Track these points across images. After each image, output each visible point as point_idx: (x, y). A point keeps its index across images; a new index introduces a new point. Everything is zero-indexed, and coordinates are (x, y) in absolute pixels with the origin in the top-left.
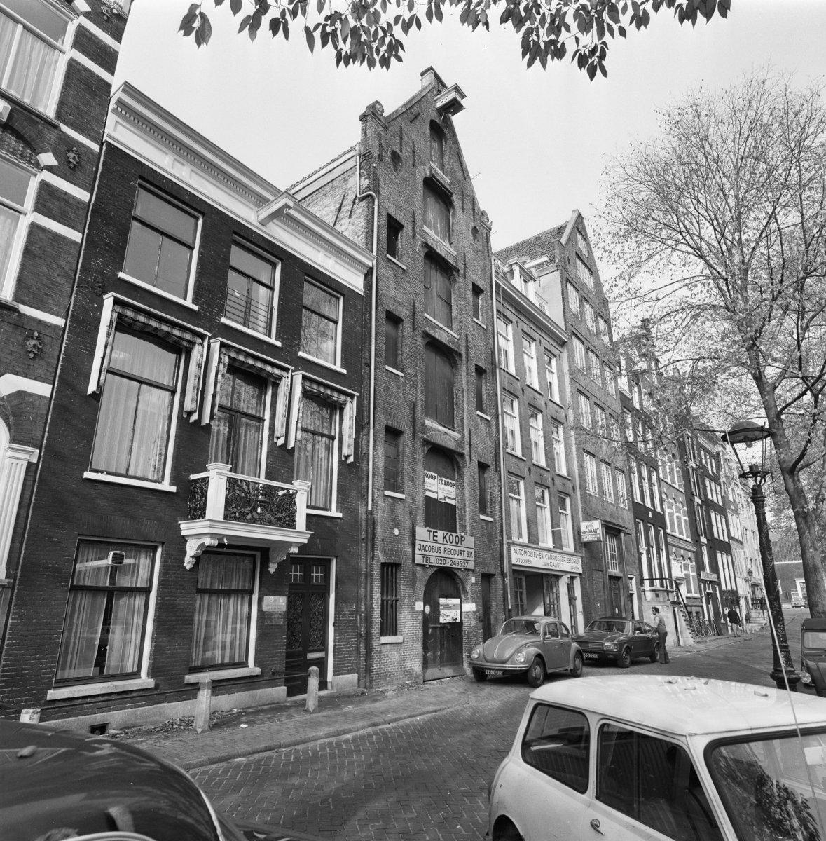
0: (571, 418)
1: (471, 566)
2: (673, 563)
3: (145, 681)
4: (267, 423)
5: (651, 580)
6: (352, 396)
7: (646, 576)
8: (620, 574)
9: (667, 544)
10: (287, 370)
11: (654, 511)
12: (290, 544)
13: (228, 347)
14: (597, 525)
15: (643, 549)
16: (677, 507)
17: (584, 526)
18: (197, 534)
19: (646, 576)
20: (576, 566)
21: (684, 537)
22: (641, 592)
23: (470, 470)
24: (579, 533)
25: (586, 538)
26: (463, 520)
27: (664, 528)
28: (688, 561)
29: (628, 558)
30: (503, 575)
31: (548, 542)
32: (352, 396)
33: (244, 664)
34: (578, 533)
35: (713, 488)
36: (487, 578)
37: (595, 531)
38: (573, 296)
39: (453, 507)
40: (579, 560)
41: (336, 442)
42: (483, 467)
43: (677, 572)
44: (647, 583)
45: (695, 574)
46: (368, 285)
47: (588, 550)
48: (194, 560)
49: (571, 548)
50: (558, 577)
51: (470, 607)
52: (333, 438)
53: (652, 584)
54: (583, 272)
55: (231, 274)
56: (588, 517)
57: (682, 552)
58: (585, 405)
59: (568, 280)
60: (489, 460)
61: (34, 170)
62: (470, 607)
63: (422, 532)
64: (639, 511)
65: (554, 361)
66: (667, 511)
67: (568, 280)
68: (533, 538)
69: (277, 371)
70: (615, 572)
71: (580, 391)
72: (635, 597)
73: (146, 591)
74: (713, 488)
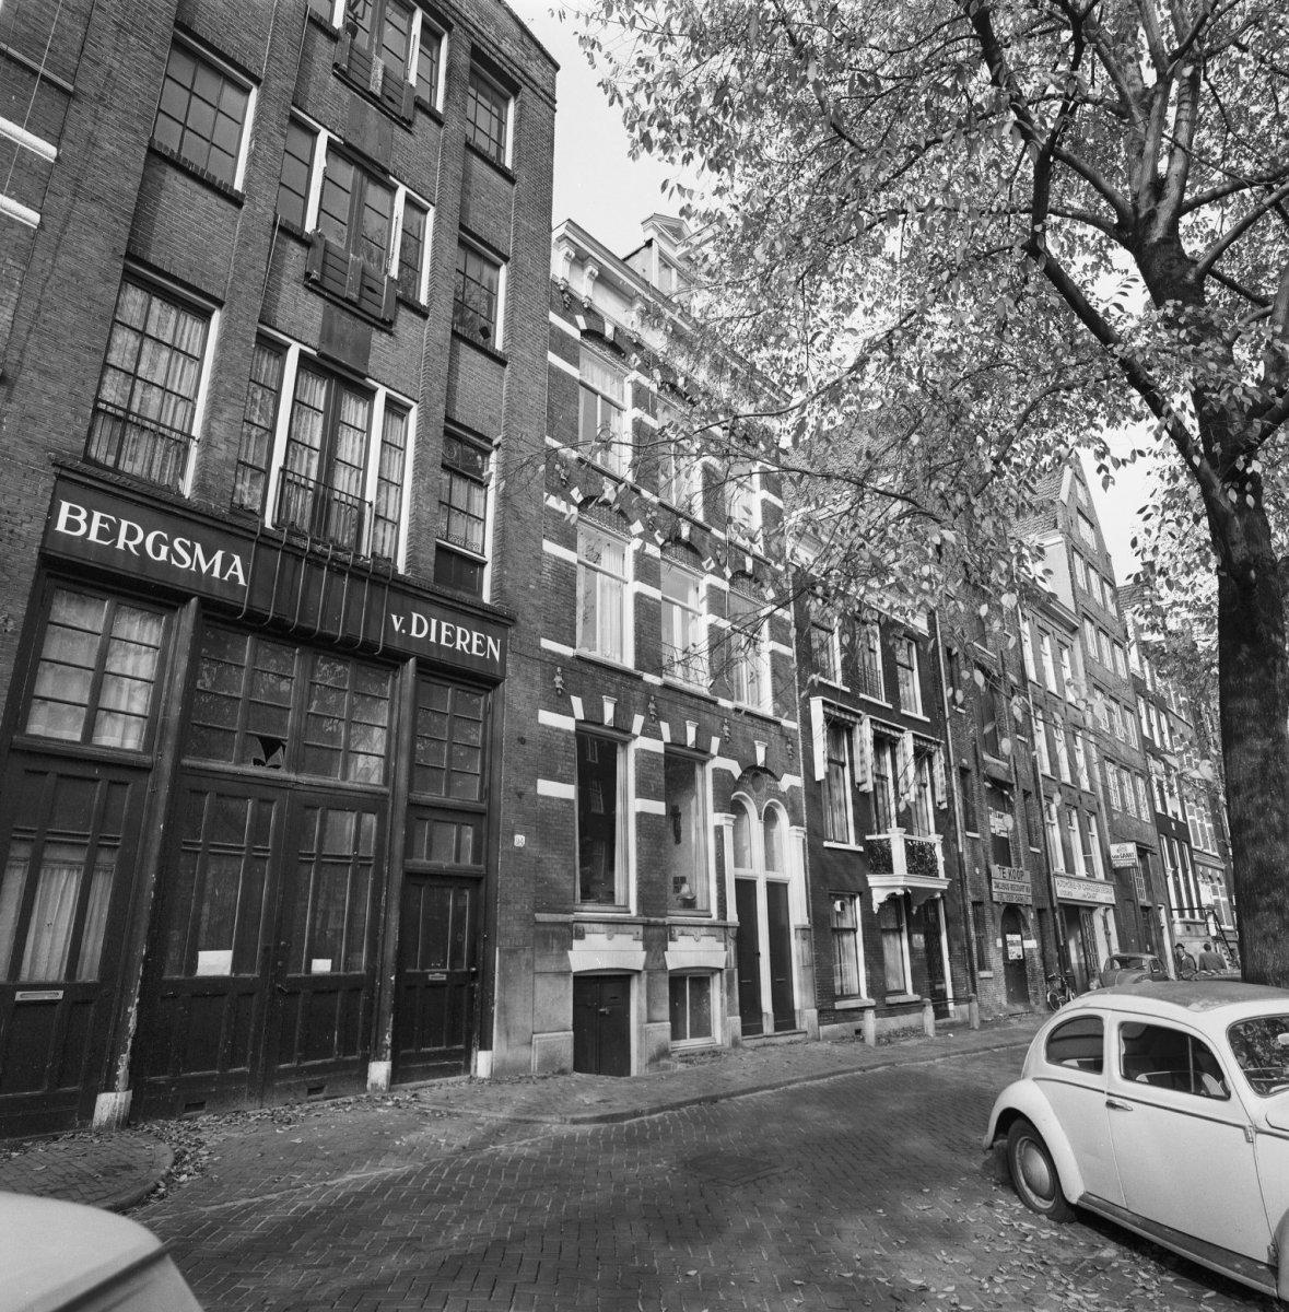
0: (1089, 722)
1: (1030, 901)
2: (1201, 886)
3: (911, 996)
4: (891, 781)
5: (1181, 910)
6: (938, 744)
7: (1174, 905)
8: (1149, 904)
9: (1193, 863)
10: (902, 731)
11: (1177, 822)
12: (936, 890)
13: (877, 723)
14: (1131, 848)
15: (1169, 868)
16: (1200, 813)
17: (1114, 849)
18: (880, 887)
19: (1174, 905)
20: (1106, 895)
21: (1210, 851)
22: (1171, 924)
23: (1016, 798)
24: (1109, 857)
25: (1118, 864)
26: (1017, 853)
27: (1189, 843)
28: (1216, 883)
29: (1154, 883)
30: (1053, 909)
31: (1081, 870)
32: (938, 744)
33: (903, 992)
34: (1107, 858)
35: (1154, 721)
36: (1040, 912)
37: (1129, 855)
38: (1079, 563)
39: (1006, 840)
40: (1111, 889)
41: (847, 769)
42: (1026, 794)
43: (1207, 898)
44: (1175, 913)
45: (1225, 899)
46: (932, 625)
47: (1117, 875)
48: (592, 890)
49: (1100, 875)
50: (1091, 909)
51: (1032, 944)
52: (843, 765)
53: (1182, 915)
54: (1084, 529)
55: (900, 669)
56: (1119, 837)
57: (1210, 871)
58: (1099, 701)
59: (1074, 549)
60: (1031, 788)
61: (699, 573)
62: (1032, 944)
63: (995, 868)
64: (1162, 822)
65: (1065, 653)
66: (1189, 818)
67: (1074, 549)
68: (1070, 867)
69: (893, 733)
70: (1144, 900)
71: (1096, 687)
72: (1166, 931)
73: (855, 931)
74: (1154, 721)
